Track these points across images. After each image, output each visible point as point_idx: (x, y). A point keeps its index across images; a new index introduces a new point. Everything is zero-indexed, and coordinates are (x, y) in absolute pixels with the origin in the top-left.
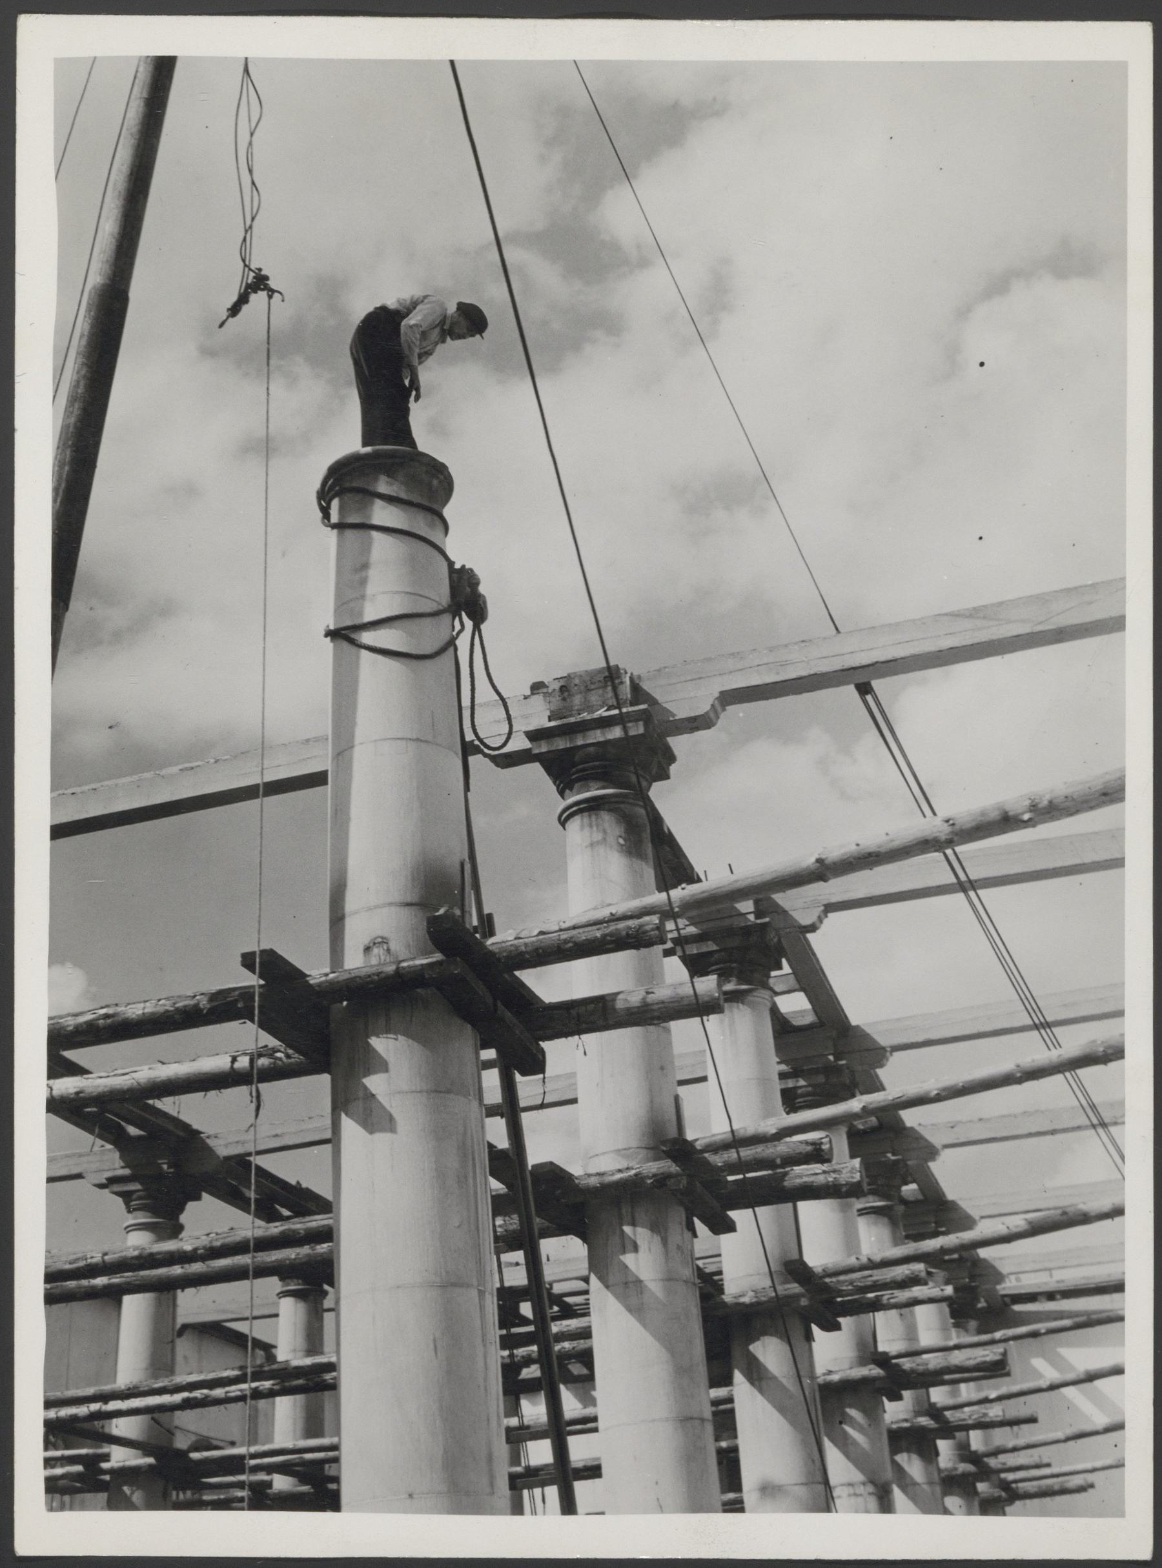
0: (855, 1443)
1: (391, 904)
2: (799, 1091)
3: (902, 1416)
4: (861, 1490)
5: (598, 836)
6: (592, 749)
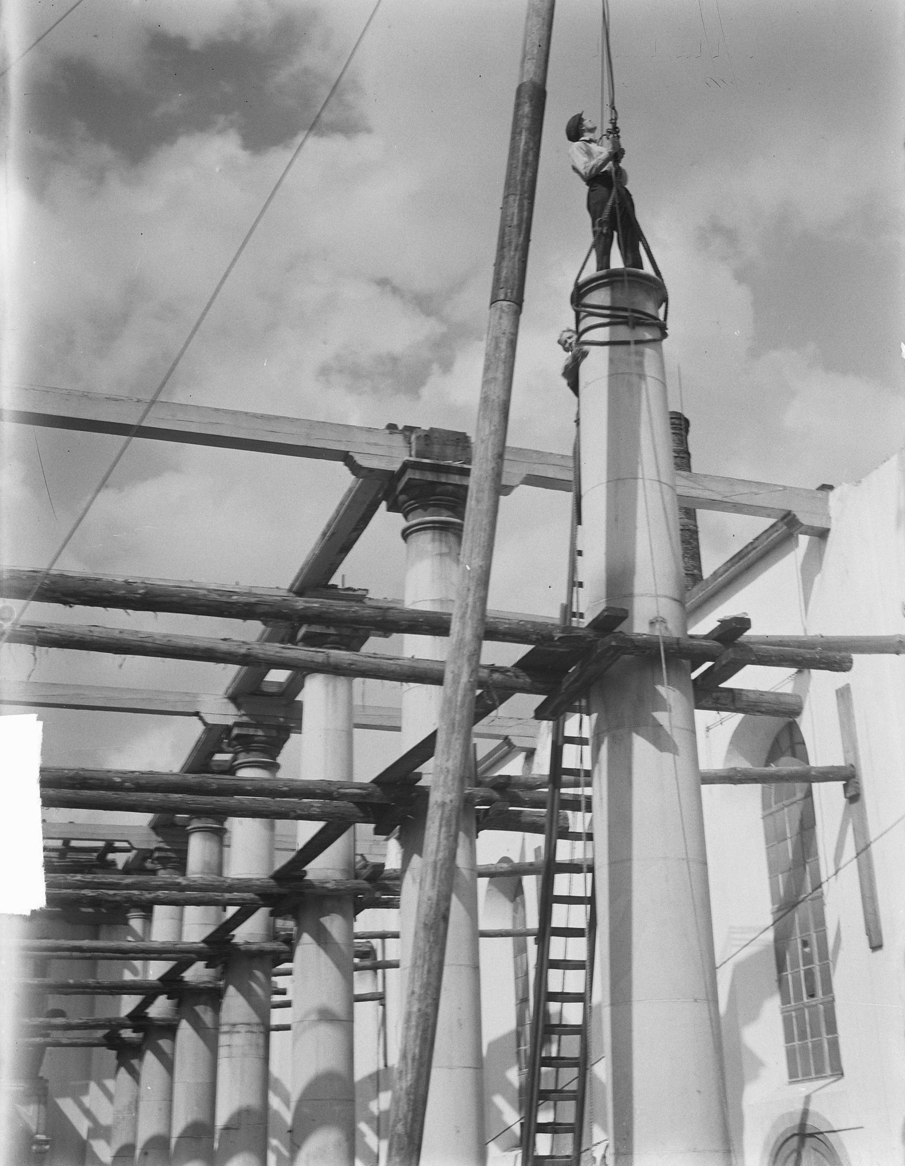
0: (257, 995)
1: (666, 596)
2: (256, 739)
3: (206, 979)
4: (255, 1029)
5: (445, 550)
6: (450, 488)
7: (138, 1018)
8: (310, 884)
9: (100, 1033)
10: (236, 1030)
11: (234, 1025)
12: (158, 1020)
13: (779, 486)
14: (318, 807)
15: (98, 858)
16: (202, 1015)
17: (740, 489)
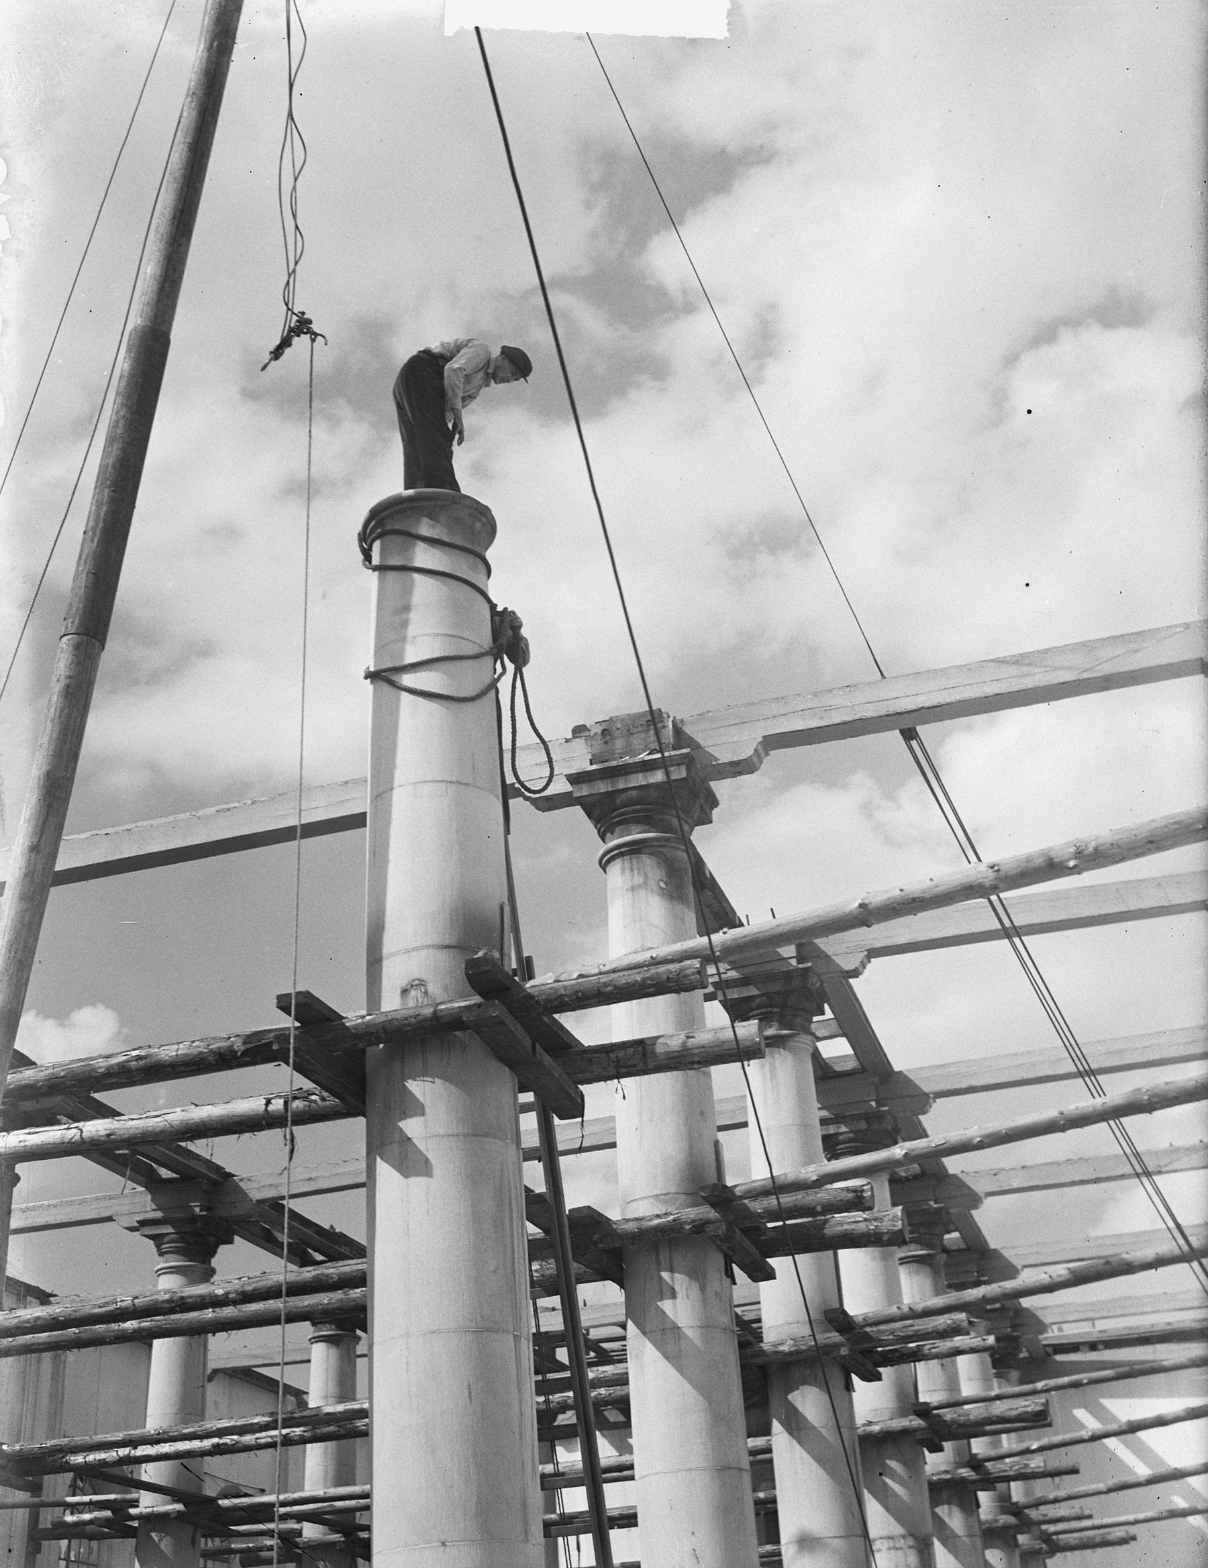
2: (841, 1138)
4: (901, 1543)
5: (638, 880)
13: (1176, 626)
16: (946, 1519)
17: (1105, 653)
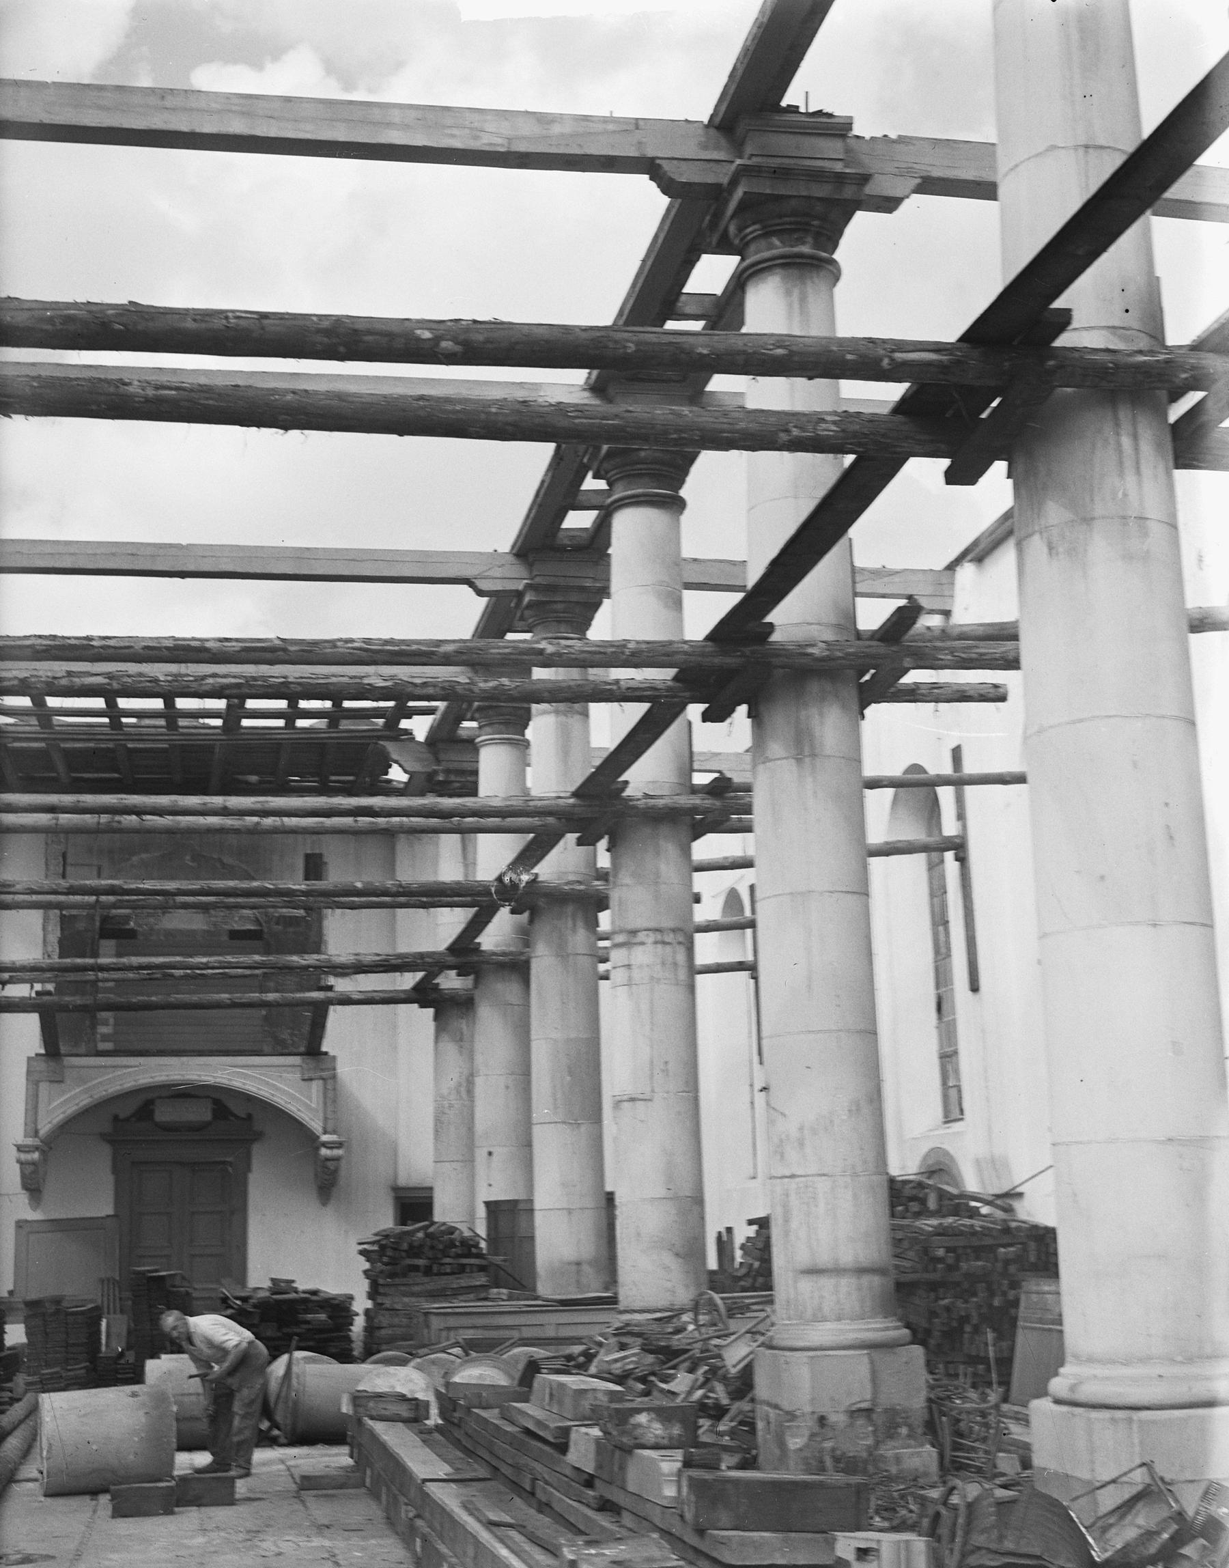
4: (669, 938)
7: (464, 953)
8: (781, 651)
9: (408, 981)
10: (635, 940)
11: (634, 932)
12: (494, 954)
14: (834, 423)
15: (387, 726)
